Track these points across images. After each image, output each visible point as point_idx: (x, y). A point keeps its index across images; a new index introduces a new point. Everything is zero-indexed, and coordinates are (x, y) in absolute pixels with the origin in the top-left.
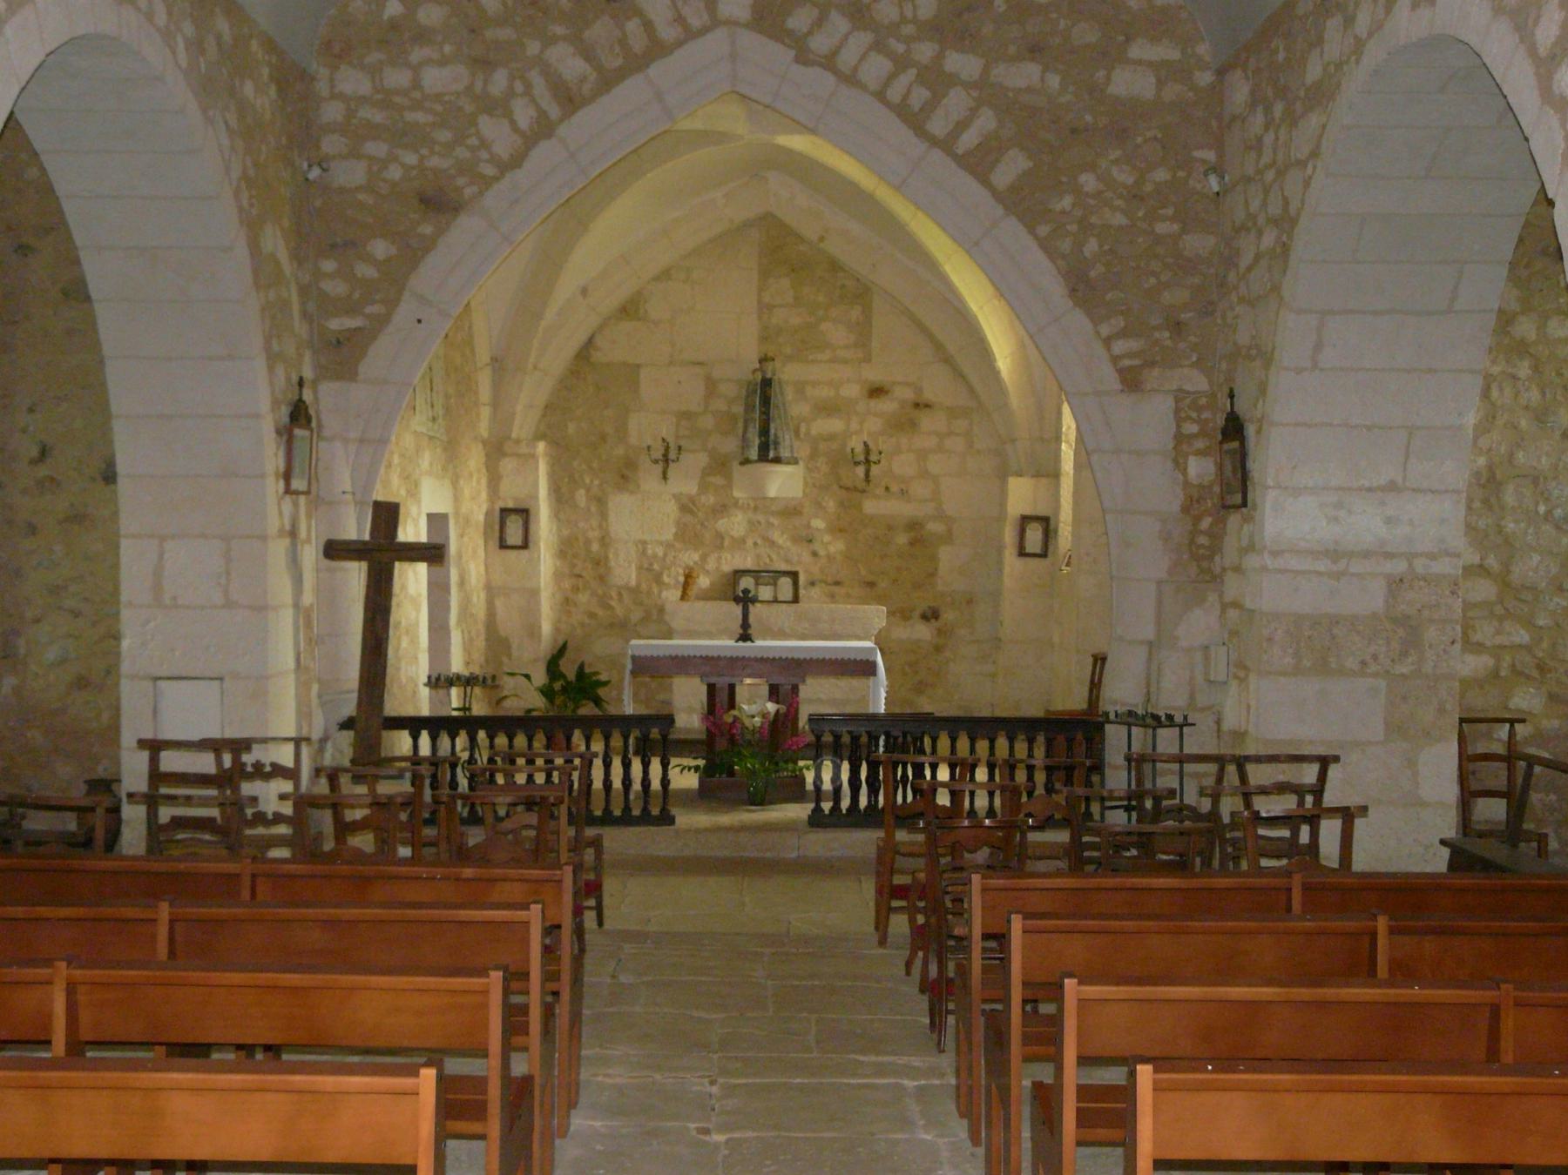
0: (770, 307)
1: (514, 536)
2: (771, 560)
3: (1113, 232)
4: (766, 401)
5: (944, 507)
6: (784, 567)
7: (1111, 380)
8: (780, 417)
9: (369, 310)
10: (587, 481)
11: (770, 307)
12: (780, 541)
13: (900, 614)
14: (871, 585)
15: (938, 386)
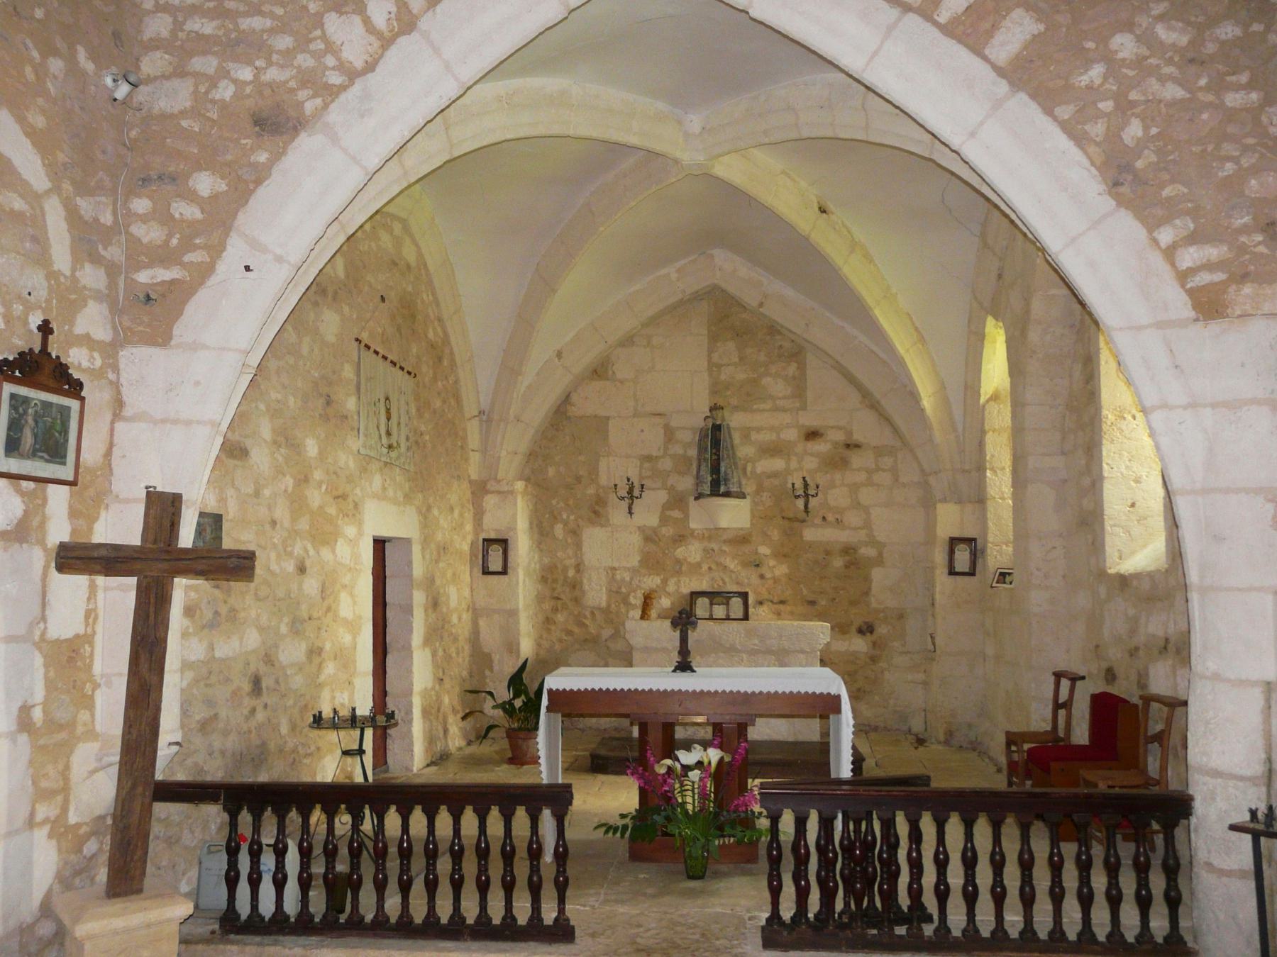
0: (719, 366)
1: (495, 563)
2: (724, 583)
3: (1164, 110)
4: (716, 443)
5: (876, 534)
6: (735, 588)
7: (1180, 305)
8: (728, 456)
9: (189, 258)
10: (565, 517)
11: (719, 366)
12: (732, 567)
13: (840, 629)
14: (812, 603)
15: (866, 428)
